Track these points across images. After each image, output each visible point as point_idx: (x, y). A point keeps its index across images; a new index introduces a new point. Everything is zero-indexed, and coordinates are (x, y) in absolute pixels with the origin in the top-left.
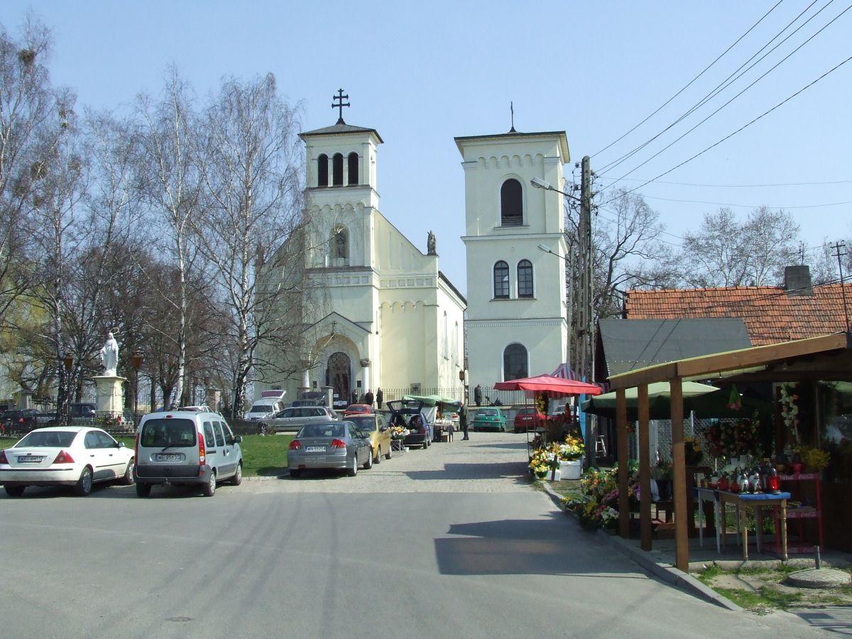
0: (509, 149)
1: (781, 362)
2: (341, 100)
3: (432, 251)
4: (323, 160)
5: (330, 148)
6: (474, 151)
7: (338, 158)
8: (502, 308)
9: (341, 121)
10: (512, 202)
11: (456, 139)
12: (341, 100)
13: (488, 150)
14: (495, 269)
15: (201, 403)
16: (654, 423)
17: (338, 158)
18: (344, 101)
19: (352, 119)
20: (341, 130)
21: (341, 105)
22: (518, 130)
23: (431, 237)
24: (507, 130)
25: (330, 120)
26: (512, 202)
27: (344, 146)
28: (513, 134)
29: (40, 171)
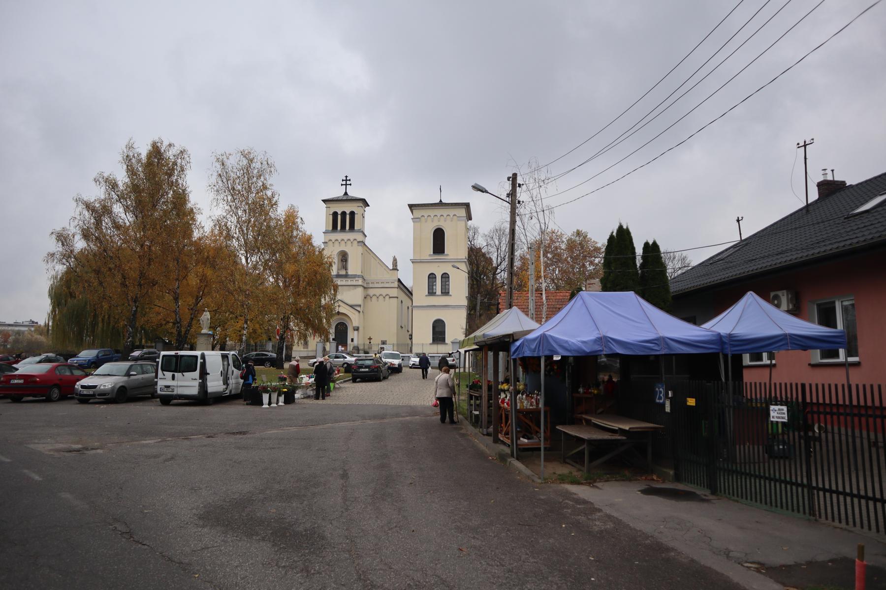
0: (439, 212)
1: (784, 566)
2: (346, 182)
3: (395, 268)
4: (335, 214)
5: (339, 208)
6: (418, 213)
7: (344, 214)
8: (433, 301)
9: (346, 194)
10: (439, 240)
11: (412, 207)
12: (346, 182)
13: (426, 212)
14: (429, 277)
15: (255, 267)
16: (501, 353)
17: (344, 214)
18: (348, 182)
19: (353, 192)
20: (346, 199)
21: (346, 185)
22: (444, 201)
23: (395, 260)
24: (438, 201)
25: (339, 193)
26: (439, 240)
27: (348, 208)
28: (441, 204)
29: (78, 443)
